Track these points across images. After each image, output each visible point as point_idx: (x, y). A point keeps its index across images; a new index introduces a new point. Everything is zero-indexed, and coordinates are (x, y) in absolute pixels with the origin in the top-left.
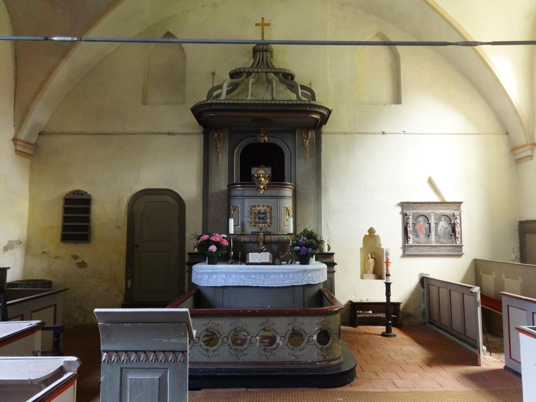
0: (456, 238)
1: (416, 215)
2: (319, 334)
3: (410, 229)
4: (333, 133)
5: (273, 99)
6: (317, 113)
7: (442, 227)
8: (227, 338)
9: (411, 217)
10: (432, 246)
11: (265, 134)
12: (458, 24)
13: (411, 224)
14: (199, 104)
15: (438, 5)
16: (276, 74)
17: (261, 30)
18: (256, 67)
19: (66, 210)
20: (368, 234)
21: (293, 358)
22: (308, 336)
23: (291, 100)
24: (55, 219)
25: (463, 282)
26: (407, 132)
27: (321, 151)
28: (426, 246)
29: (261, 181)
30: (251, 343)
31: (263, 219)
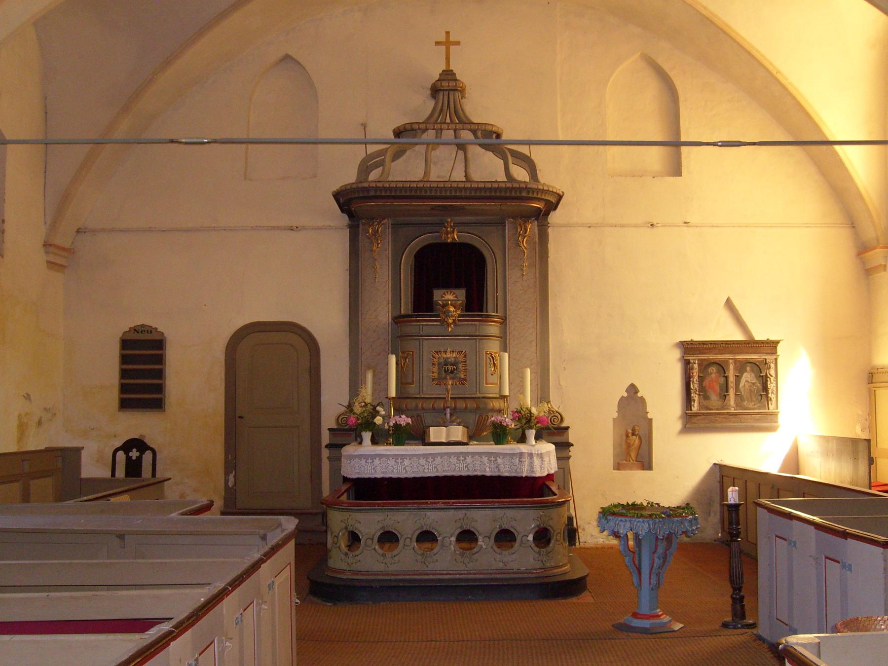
0: (768, 399)
1: (705, 363)
2: (537, 532)
3: (695, 386)
4: (568, 226)
6: (539, 200)
7: (747, 381)
8: (411, 539)
9: (696, 366)
11: (453, 227)
12: (763, 56)
13: (696, 377)
14: (348, 187)
15: (729, 27)
19: (125, 359)
20: (625, 395)
21: (501, 565)
23: (496, 182)
24: (107, 371)
25: (780, 471)
27: (547, 257)
28: (719, 414)
30: (443, 546)
31: (452, 372)
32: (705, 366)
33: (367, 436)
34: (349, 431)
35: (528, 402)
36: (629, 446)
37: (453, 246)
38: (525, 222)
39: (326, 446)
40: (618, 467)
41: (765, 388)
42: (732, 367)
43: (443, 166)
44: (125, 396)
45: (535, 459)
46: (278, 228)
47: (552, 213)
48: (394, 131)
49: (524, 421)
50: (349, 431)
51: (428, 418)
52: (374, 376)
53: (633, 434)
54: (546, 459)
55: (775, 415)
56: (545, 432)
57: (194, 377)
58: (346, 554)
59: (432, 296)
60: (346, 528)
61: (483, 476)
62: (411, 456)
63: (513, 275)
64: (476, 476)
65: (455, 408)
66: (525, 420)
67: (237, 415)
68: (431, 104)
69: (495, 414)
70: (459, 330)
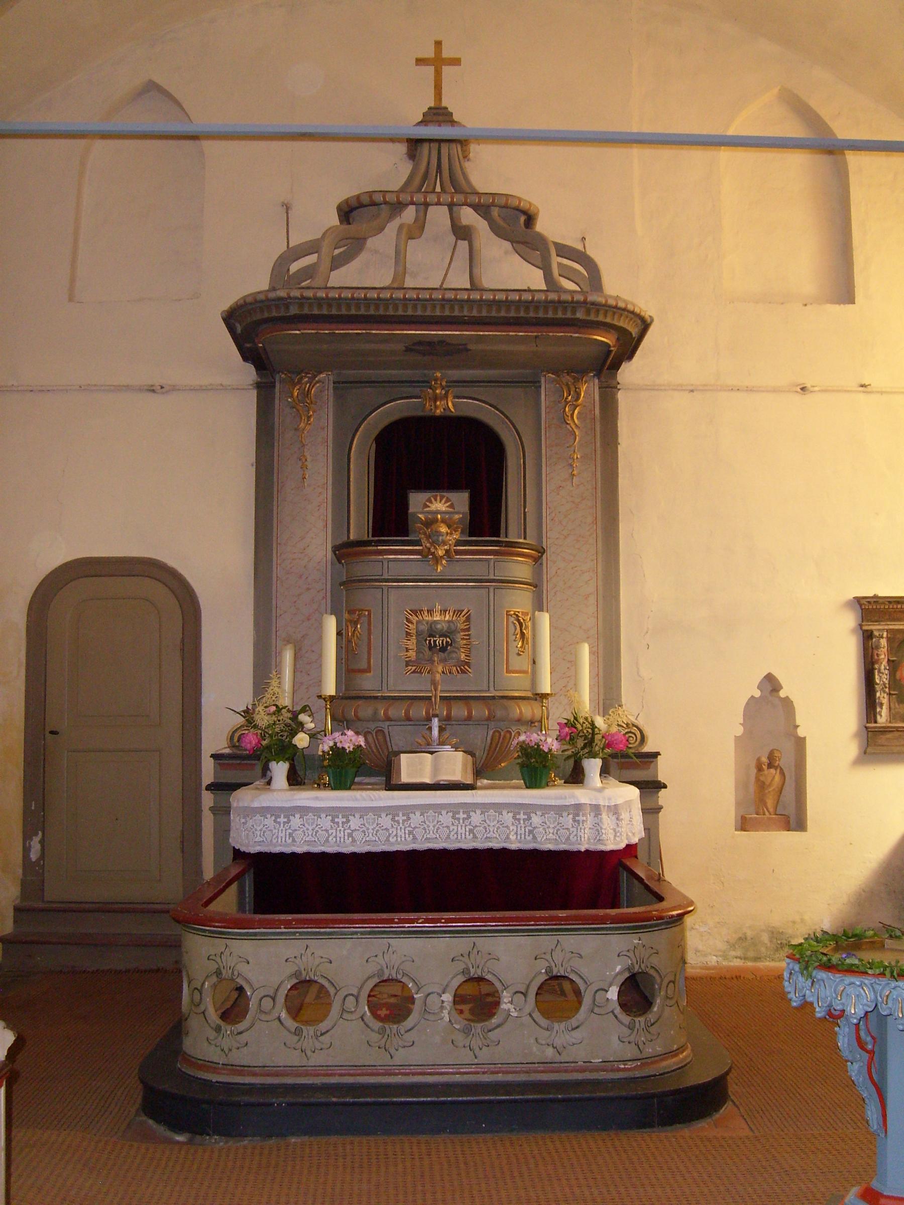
3: (882, 678)
4: (654, 388)
5: (475, 286)
8: (357, 998)
9: (884, 642)
13: (885, 663)
14: (249, 300)
16: (482, 209)
17: (432, 77)
18: (419, 190)
20: (757, 694)
21: (550, 1052)
22: (594, 987)
23: (529, 290)
26: (875, 379)
29: (439, 534)
31: (443, 649)
33: (280, 770)
34: (256, 754)
36: (762, 786)
37: (447, 415)
38: (576, 380)
39: (208, 788)
40: (744, 824)
43: (431, 265)
45: (604, 816)
46: (128, 388)
47: (625, 366)
48: (339, 209)
49: (580, 743)
50: (247, 761)
51: (398, 736)
52: (296, 658)
53: (770, 766)
54: (624, 815)
56: (613, 762)
58: (218, 1029)
59: (405, 505)
60: (218, 973)
61: (504, 850)
62: (364, 811)
64: (490, 851)
65: (448, 718)
66: (581, 740)
67: (48, 729)
68: (406, 168)
69: (523, 729)
70: (458, 570)
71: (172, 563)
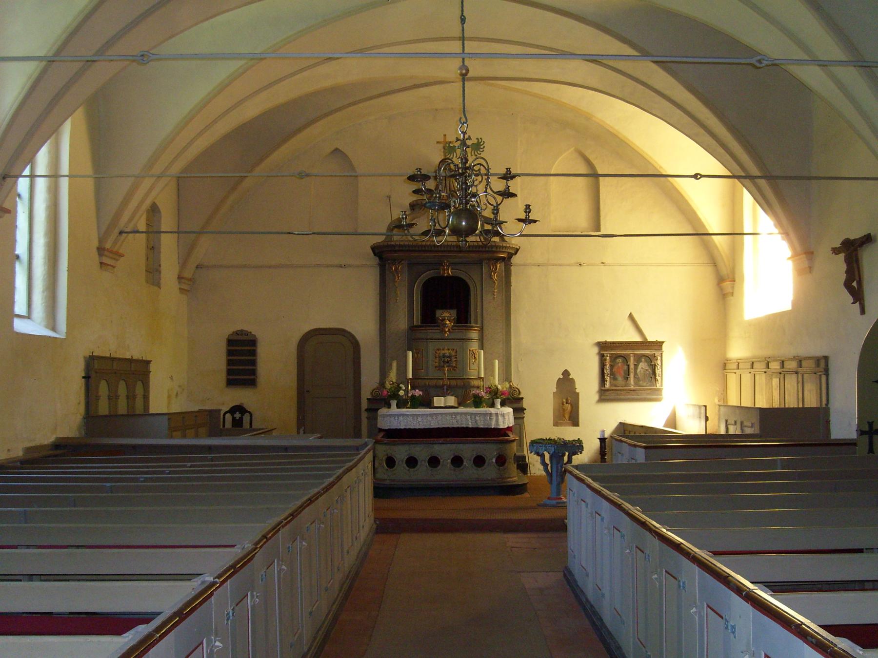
0: (656, 380)
3: (607, 371)
4: (525, 265)
6: (504, 252)
9: (608, 358)
10: (630, 390)
13: (608, 366)
19: (230, 353)
24: (218, 361)
32: (614, 358)
33: (394, 403)
35: (497, 383)
39: (366, 410)
41: (654, 373)
42: (632, 358)
44: (231, 377)
50: (380, 400)
54: (507, 417)
55: (660, 390)
57: (276, 363)
59: (435, 315)
63: (487, 297)
66: (494, 393)
71: (350, 330)
